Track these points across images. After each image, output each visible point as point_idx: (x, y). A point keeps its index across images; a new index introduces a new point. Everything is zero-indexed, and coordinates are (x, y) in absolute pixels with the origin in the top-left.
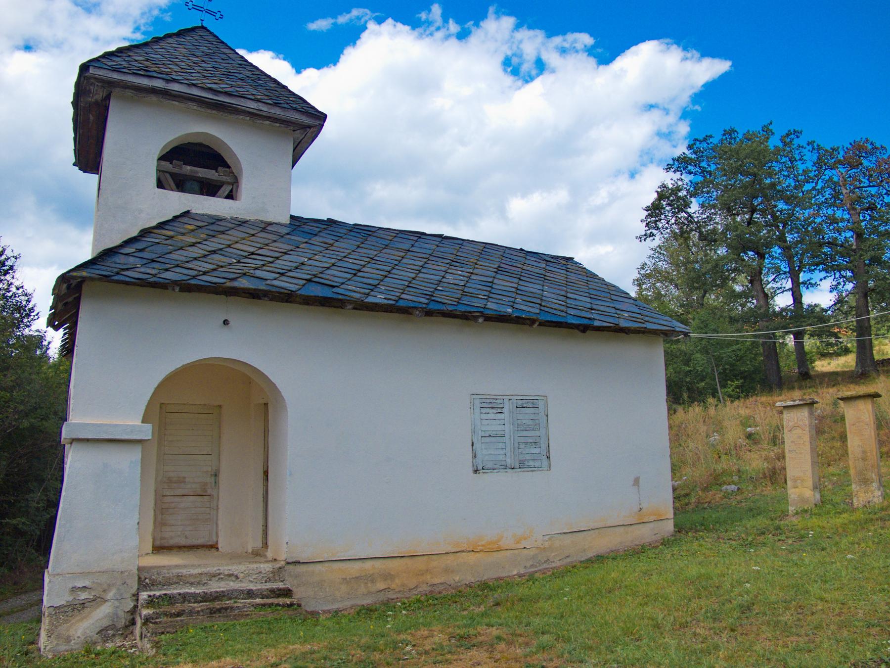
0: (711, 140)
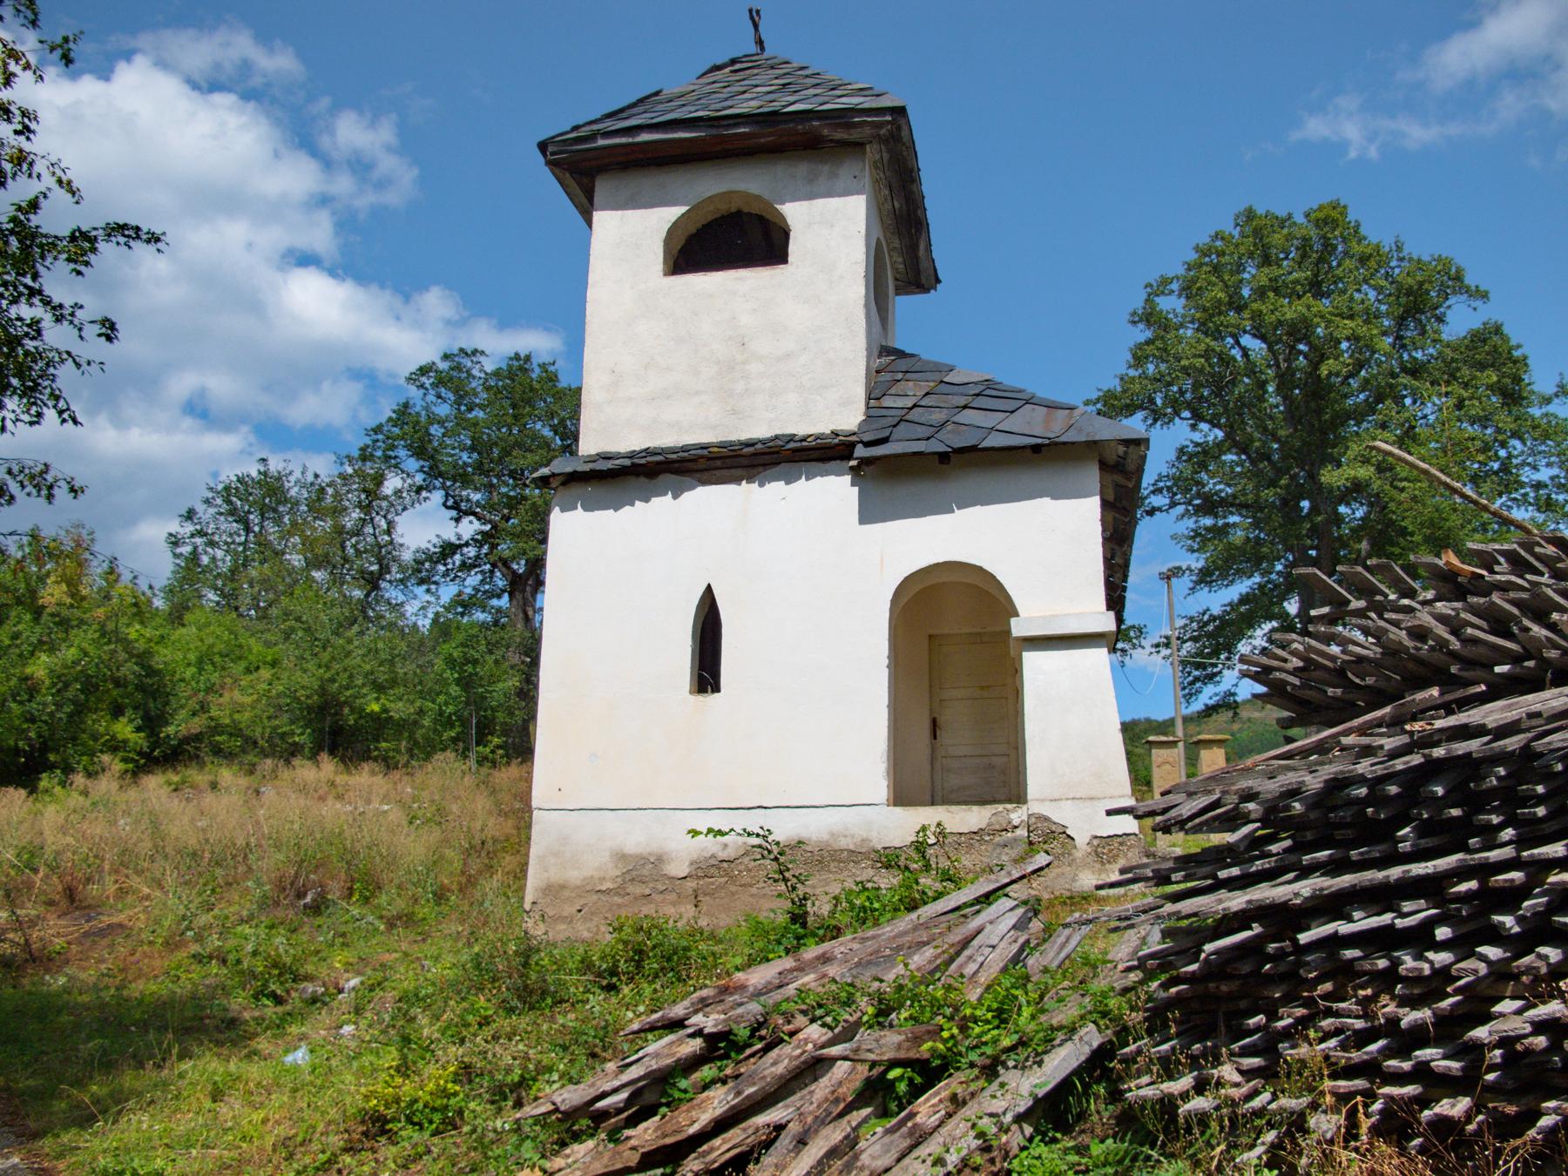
0: (482, 359)
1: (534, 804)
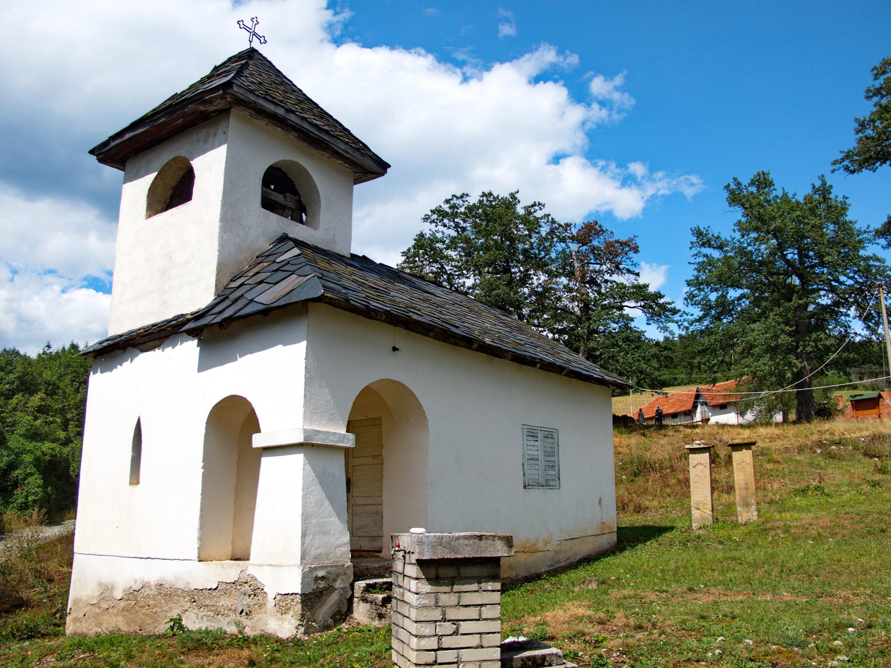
0: (467, 198)
1: (75, 550)
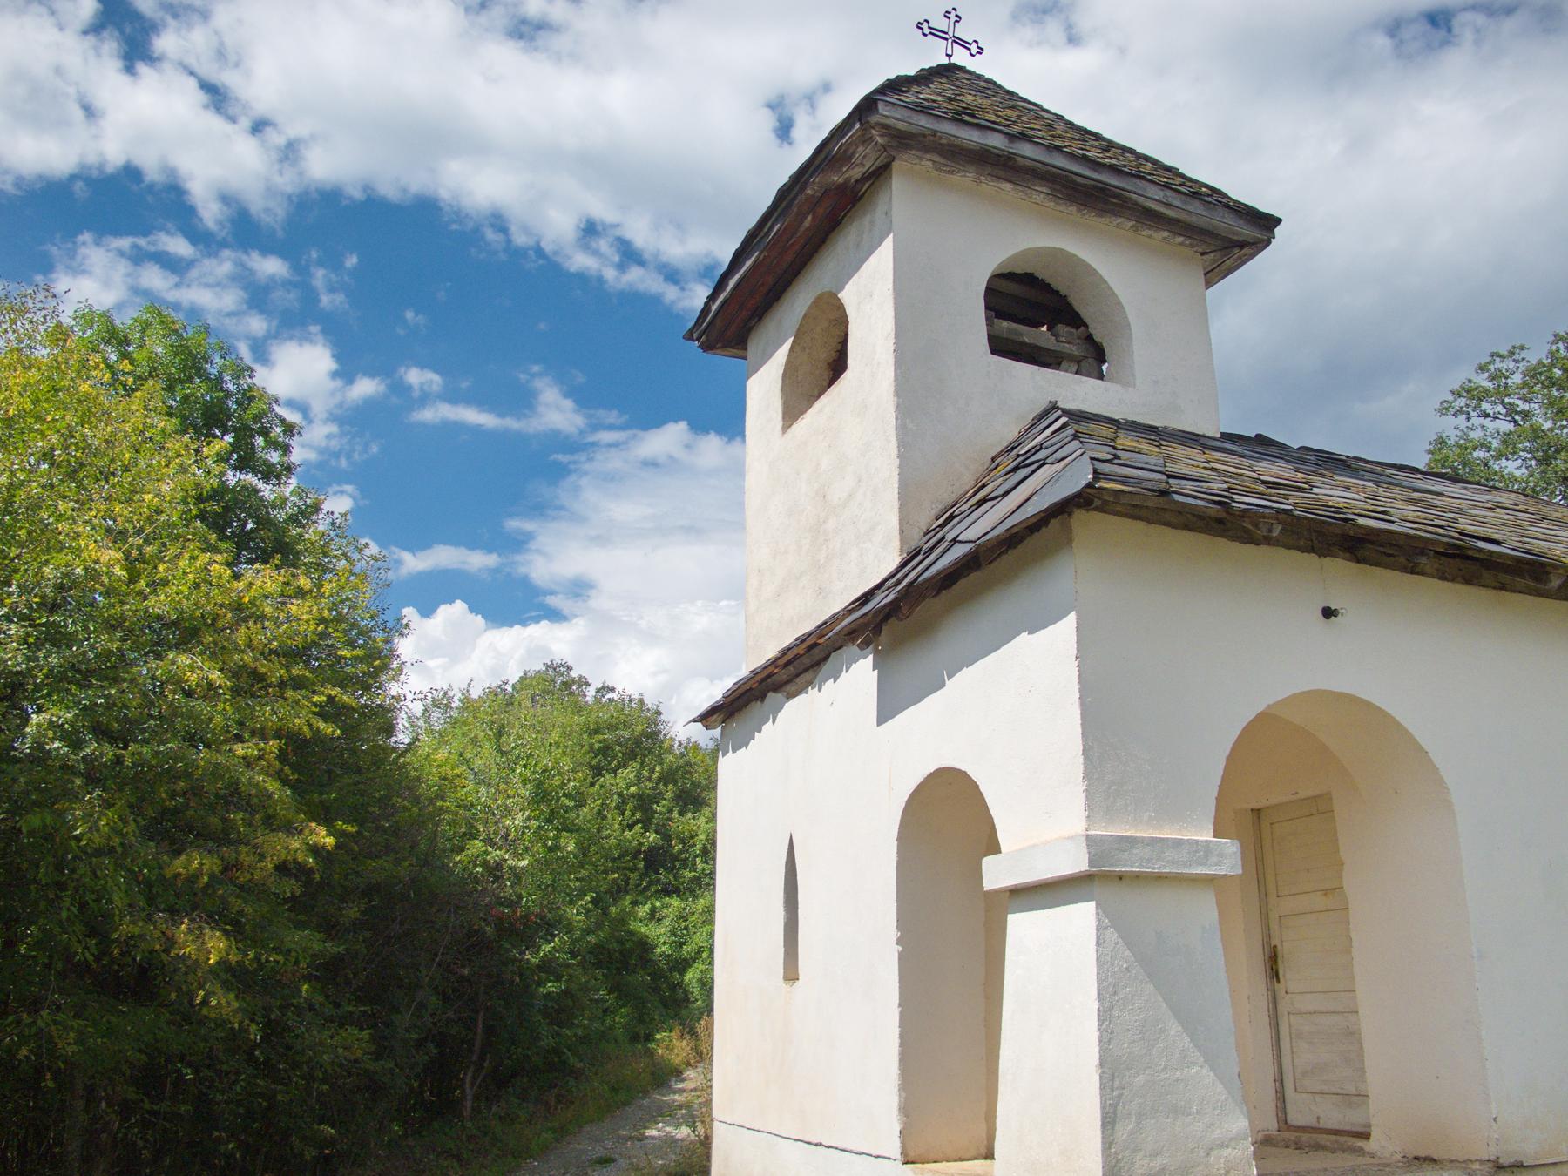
0: (1523, 354)
